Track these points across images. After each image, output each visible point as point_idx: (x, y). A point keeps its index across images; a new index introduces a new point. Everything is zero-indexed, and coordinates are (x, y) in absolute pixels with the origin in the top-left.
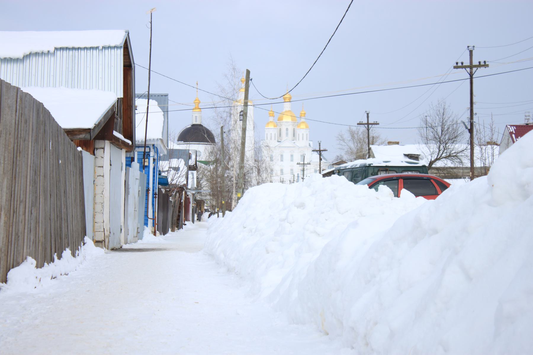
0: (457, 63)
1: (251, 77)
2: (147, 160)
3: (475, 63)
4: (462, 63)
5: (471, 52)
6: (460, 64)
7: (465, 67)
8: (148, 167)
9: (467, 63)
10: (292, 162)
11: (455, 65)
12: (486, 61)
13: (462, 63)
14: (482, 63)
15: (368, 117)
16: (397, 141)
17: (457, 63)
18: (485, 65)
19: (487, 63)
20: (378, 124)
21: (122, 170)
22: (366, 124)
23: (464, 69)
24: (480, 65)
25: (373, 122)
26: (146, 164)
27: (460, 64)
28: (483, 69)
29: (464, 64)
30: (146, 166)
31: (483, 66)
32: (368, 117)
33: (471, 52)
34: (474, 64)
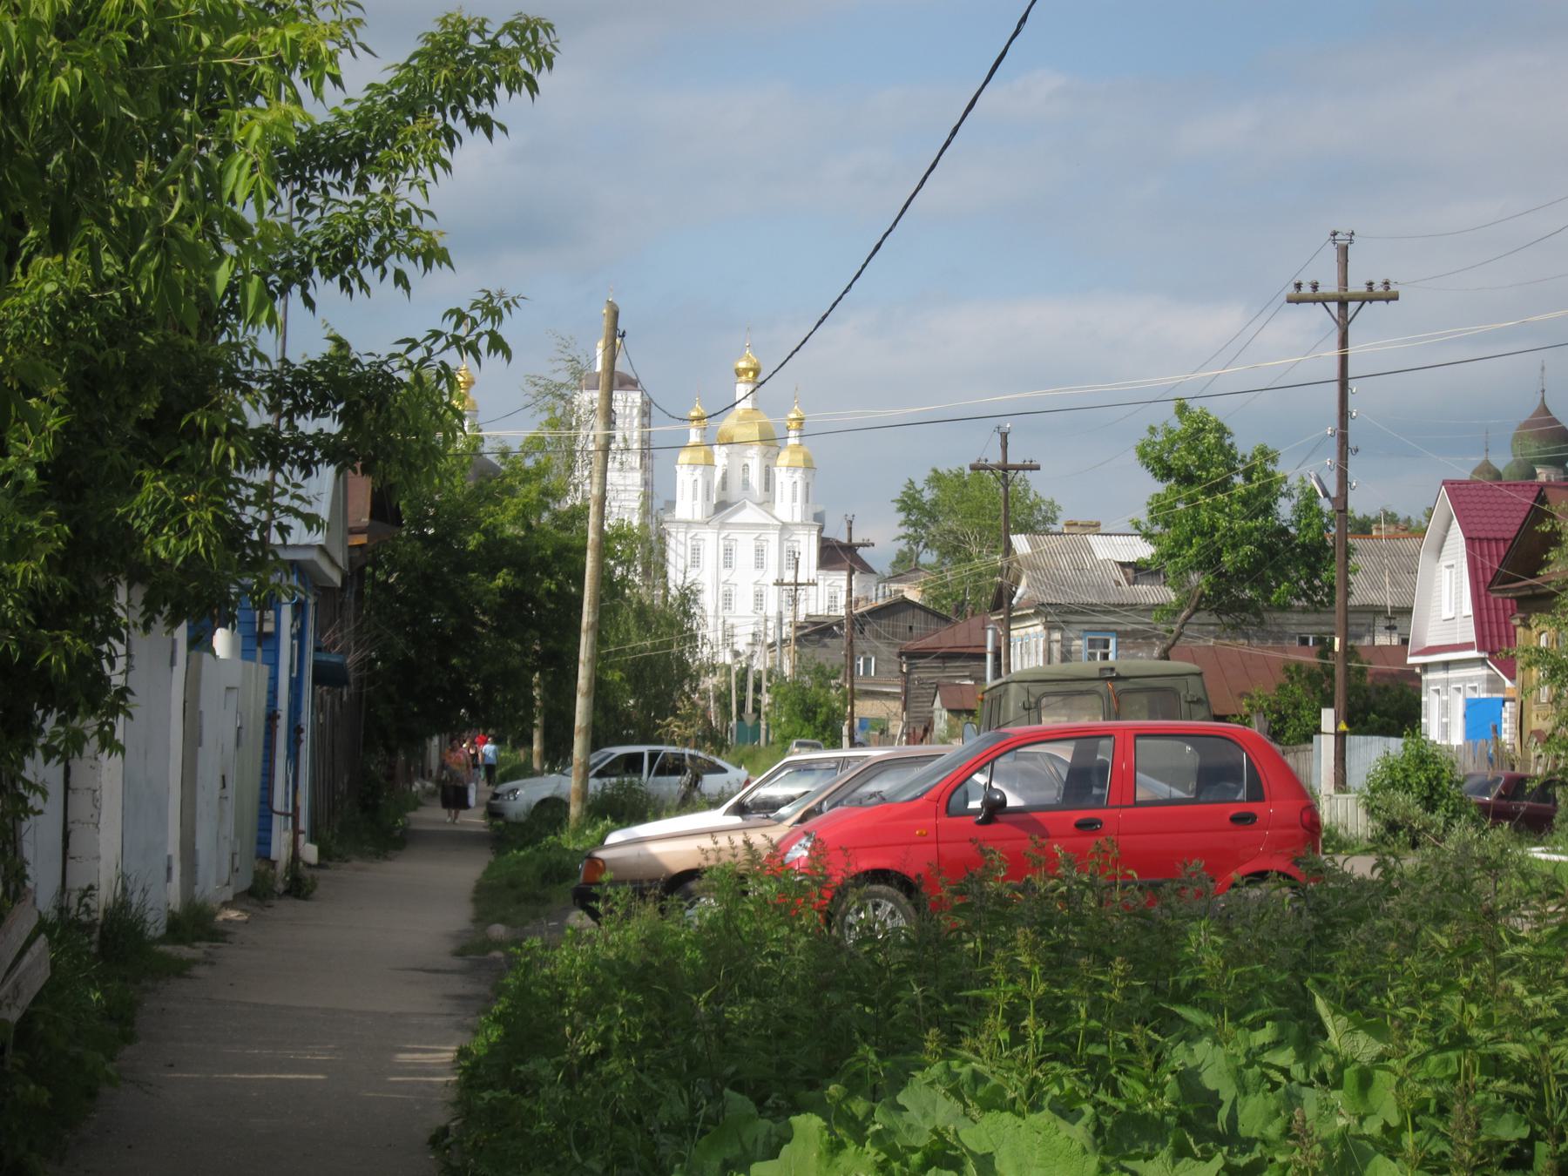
0: (1298, 286)
1: (621, 326)
2: (270, 614)
3: (1356, 285)
4: (1315, 287)
5: (1344, 252)
6: (1306, 290)
7: (1324, 300)
8: (274, 637)
9: (1330, 286)
10: (761, 572)
11: (1291, 290)
12: (1392, 280)
13: (1315, 287)
14: (1378, 288)
15: (1005, 446)
16: (1095, 520)
17: (1298, 286)
18: (1371, 284)
19: (1393, 288)
20: (1038, 468)
21: (172, 663)
22: (999, 467)
23: (1319, 305)
24: (1369, 297)
25: (1019, 462)
26: (268, 627)
27: (1306, 290)
28: (1379, 305)
29: (1321, 290)
30: (268, 636)
31: (1379, 298)
32: (1005, 446)
33: (1344, 252)
34: (1351, 289)
